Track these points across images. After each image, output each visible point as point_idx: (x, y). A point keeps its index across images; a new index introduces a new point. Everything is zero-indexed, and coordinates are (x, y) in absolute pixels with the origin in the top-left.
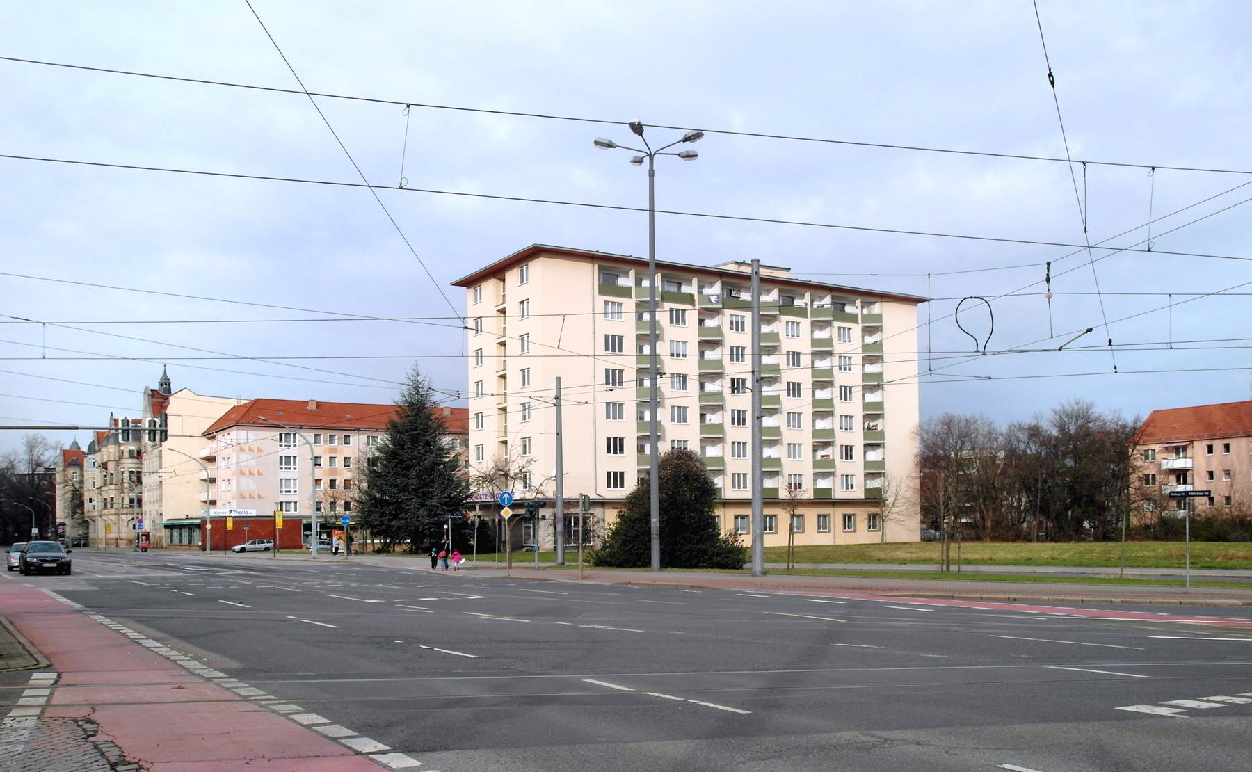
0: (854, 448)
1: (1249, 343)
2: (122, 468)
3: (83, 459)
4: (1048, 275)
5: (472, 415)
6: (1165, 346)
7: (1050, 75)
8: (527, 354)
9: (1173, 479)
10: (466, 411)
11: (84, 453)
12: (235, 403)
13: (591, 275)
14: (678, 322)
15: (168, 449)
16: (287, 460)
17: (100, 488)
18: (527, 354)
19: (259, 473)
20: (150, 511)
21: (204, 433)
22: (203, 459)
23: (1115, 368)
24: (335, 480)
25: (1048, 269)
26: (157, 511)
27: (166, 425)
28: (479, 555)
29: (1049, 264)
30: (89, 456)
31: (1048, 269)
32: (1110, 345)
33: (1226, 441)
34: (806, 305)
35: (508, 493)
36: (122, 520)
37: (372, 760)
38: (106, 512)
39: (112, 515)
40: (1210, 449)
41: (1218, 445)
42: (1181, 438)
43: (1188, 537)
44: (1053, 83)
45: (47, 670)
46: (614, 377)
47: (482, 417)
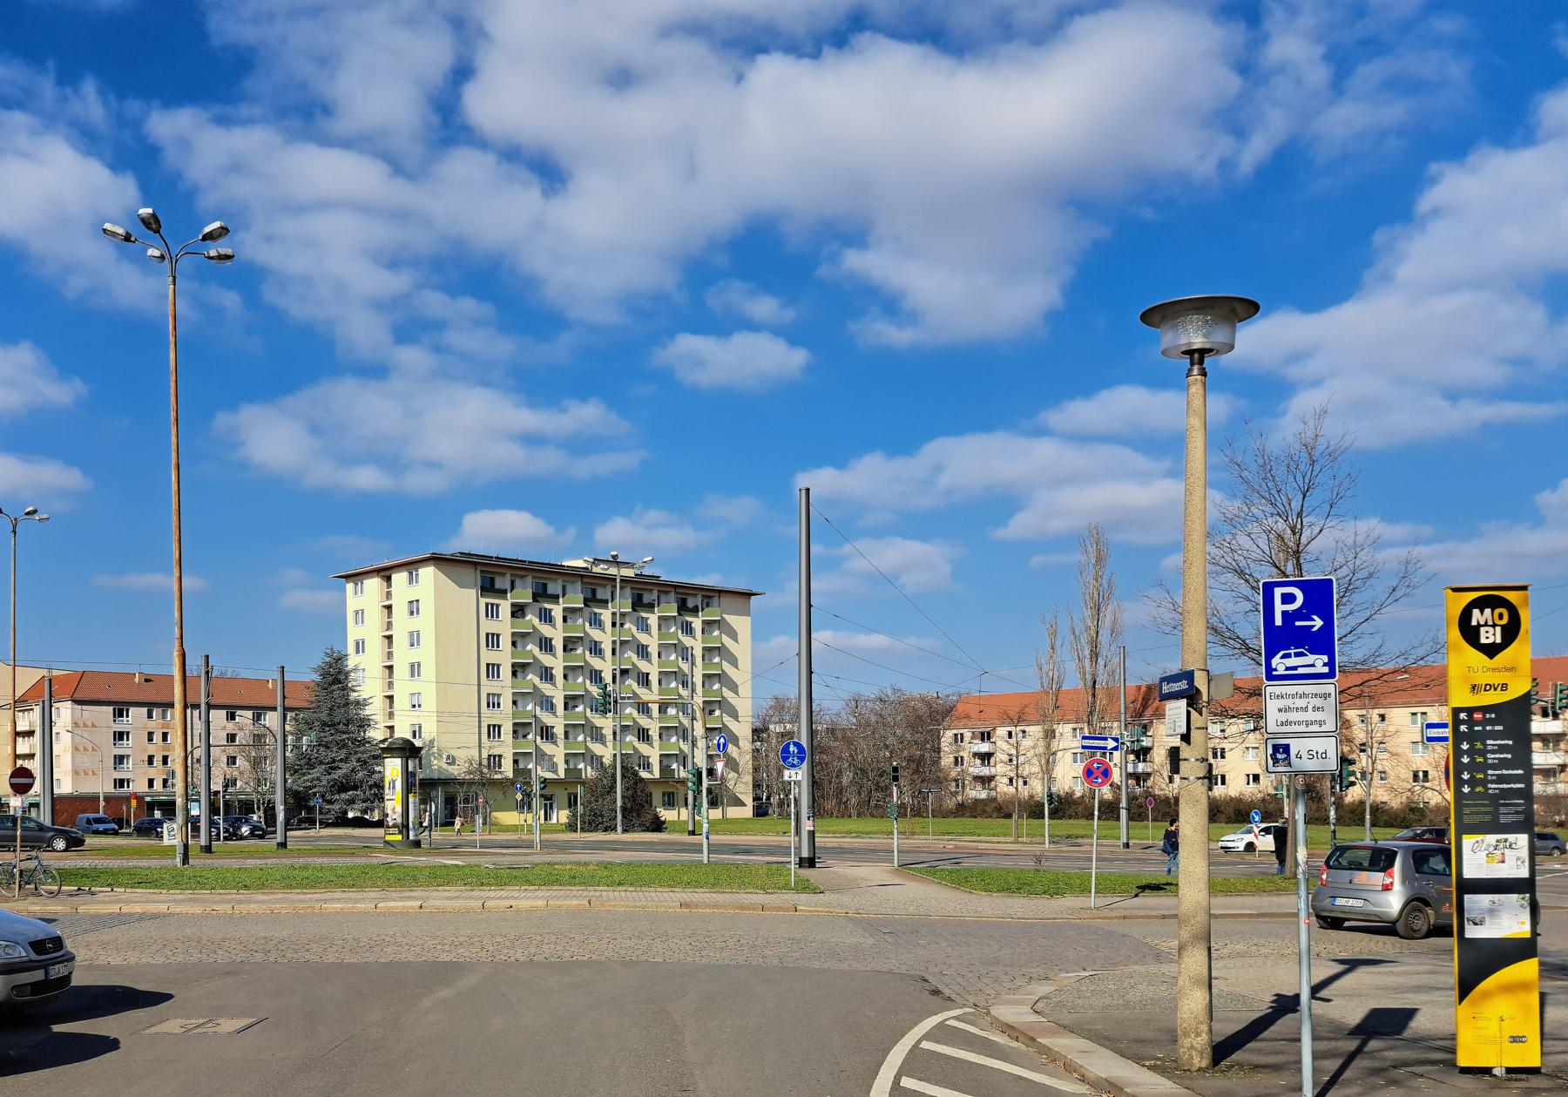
9: (978, 762)
16: (119, 736)
46: (493, 670)
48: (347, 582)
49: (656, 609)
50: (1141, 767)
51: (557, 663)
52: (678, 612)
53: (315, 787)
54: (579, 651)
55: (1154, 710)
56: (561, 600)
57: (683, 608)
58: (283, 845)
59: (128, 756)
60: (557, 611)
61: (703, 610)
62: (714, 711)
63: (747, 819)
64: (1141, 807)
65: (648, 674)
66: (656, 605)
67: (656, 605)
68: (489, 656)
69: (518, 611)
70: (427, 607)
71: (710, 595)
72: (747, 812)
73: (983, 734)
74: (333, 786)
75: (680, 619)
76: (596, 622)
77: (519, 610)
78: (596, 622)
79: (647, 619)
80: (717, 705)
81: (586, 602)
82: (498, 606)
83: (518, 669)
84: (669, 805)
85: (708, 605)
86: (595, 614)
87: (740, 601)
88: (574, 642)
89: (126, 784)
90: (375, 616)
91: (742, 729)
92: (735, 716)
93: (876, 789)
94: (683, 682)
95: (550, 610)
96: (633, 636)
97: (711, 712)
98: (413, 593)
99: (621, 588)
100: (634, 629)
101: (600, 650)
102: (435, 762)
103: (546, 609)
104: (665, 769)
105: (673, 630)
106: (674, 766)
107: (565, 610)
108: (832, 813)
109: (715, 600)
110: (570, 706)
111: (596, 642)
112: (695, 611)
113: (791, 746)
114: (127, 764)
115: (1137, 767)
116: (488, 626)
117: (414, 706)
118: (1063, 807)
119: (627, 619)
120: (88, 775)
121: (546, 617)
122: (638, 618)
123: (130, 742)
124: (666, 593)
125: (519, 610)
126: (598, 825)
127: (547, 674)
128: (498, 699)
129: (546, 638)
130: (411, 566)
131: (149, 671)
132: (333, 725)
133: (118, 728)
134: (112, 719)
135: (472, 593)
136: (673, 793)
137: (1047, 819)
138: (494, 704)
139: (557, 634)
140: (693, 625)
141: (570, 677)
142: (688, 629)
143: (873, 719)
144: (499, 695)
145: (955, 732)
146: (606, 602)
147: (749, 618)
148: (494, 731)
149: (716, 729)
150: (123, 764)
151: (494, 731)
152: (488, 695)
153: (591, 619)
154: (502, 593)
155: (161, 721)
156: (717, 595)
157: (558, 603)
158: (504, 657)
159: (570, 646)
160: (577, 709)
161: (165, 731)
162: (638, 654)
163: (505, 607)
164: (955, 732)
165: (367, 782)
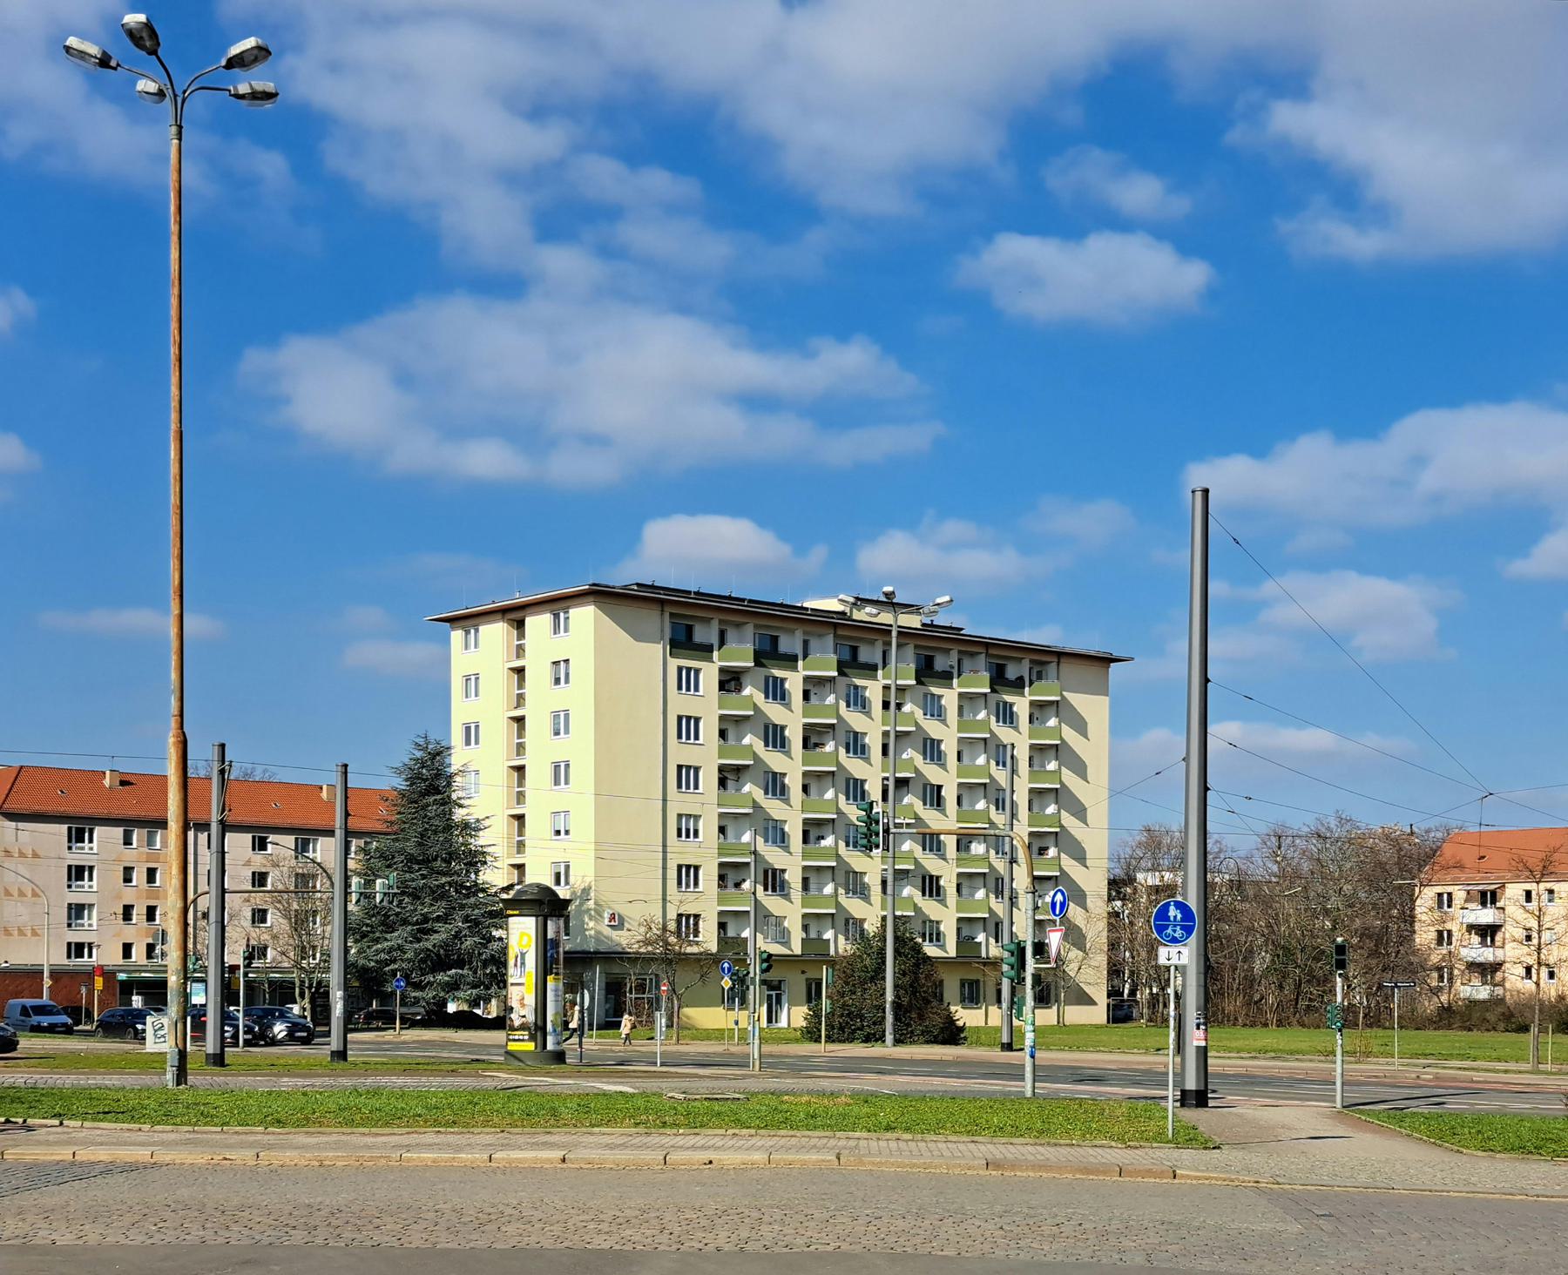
14: (688, 689)
33: (1528, 886)
34: (952, 667)
46: (687, 775)
48: (453, 629)
51: (792, 766)
57: (999, 679)
58: (341, 1055)
59: (91, 906)
60: (794, 681)
61: (1031, 683)
62: (1047, 849)
63: (1097, 1027)
65: (940, 787)
66: (955, 674)
67: (955, 674)
68: (681, 753)
69: (730, 681)
71: (1044, 659)
72: (1098, 1014)
73: (1483, 894)
75: (994, 698)
81: (842, 667)
82: (697, 671)
83: (728, 776)
85: (1040, 677)
86: (856, 687)
87: (1089, 672)
89: (86, 950)
90: (497, 685)
92: (1080, 857)
97: (1042, 851)
98: (560, 647)
99: (899, 646)
100: (919, 713)
106: (981, 938)
108: (1236, 1019)
111: (856, 734)
112: (1018, 685)
113: (1172, 908)
114: (89, 918)
116: (682, 704)
117: (558, 833)
121: (776, 691)
122: (925, 695)
123: (94, 883)
124: (972, 655)
126: (854, 1031)
129: (775, 726)
130: (557, 604)
131: (129, 767)
133: (76, 859)
134: (66, 844)
135: (655, 651)
136: (977, 981)
138: (688, 831)
139: (793, 721)
140: (1015, 709)
141: (813, 789)
143: (1306, 866)
144: (697, 818)
145: (1439, 889)
146: (874, 668)
152: (680, 816)
153: (848, 696)
155: (146, 850)
158: (707, 754)
159: (814, 740)
162: (924, 754)
163: (709, 674)
164: (1439, 889)
165: (480, 954)
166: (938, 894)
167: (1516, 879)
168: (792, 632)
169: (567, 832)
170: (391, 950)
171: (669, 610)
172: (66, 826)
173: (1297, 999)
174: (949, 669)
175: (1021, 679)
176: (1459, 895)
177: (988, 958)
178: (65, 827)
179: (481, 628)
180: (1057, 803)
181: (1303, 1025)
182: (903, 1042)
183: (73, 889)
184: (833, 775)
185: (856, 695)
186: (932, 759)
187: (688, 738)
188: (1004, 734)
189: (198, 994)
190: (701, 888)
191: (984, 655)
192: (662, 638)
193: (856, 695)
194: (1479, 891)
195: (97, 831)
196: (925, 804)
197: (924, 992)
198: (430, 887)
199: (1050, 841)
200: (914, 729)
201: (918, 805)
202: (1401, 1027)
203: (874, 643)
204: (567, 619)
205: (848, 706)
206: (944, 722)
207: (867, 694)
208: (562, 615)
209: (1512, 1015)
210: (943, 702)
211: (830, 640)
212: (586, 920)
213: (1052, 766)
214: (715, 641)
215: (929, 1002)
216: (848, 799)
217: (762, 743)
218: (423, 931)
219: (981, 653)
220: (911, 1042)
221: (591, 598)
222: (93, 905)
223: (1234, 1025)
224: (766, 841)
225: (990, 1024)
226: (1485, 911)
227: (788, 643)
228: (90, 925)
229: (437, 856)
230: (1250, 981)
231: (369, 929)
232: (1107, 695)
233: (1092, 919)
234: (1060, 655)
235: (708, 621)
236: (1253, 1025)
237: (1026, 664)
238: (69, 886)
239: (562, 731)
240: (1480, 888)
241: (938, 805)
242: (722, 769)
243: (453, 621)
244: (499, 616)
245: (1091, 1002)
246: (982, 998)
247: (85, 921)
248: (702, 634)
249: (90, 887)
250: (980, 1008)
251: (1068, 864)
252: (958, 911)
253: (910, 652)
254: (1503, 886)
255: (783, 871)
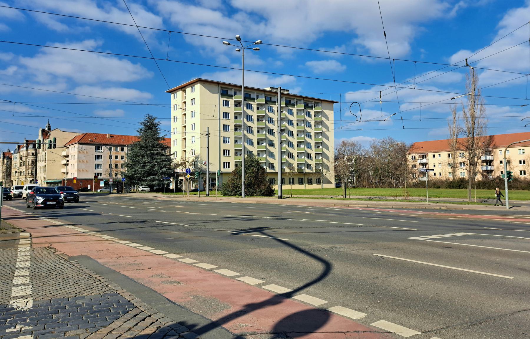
0: (230, 164)
1: (526, 264)
2: (29, 159)
3: (11, 156)
4: (381, 95)
5: (172, 141)
6: (419, 120)
7: (385, 33)
8: (194, 118)
9: (421, 166)
10: (170, 139)
11: (12, 154)
12: (78, 134)
13: (218, 90)
15: (51, 152)
16: (98, 157)
17: (19, 168)
18: (194, 118)
19: (87, 162)
20: (40, 176)
21: (64, 146)
22: (63, 156)
23: (404, 127)
24: (117, 165)
25: (381, 93)
26: (43, 176)
27: (56, 142)
28: (166, 193)
29: (381, 92)
30: (15, 155)
31: (381, 93)
32: (402, 119)
34: (295, 103)
35: (189, 169)
36: (28, 180)
37: (163, 256)
38: (20, 177)
39: (24, 178)
40: (434, 156)
41: (437, 154)
42: (424, 152)
43: (427, 182)
44: (385, 35)
45: (23, 232)
46: (226, 127)
47: (176, 141)
48: (172, 94)
49: (296, 106)
50: (489, 168)
51: (254, 125)
52: (304, 107)
53: (136, 174)
54: (264, 121)
55: (493, 145)
56: (256, 100)
57: (307, 106)
58: (208, 195)
59: (101, 164)
60: (254, 105)
61: (315, 107)
62: (319, 146)
63: (333, 188)
64: (498, 183)
65: (292, 132)
66: (296, 105)
67: (296, 105)
68: (224, 122)
69: (237, 104)
70: (197, 101)
71: (318, 102)
72: (333, 186)
73: (423, 156)
74: (144, 173)
75: (305, 110)
76: (271, 110)
77: (239, 104)
78: (271, 110)
79: (292, 110)
80: (320, 144)
81: (266, 102)
82: (228, 102)
83: (237, 127)
84: (301, 183)
85: (317, 106)
86: (271, 107)
87: (329, 105)
88: (262, 118)
89: (100, 175)
91: (331, 154)
92: (327, 148)
93: (383, 177)
94: (307, 135)
95: (251, 105)
96: (286, 116)
97: (318, 147)
98: (192, 96)
99: (281, 97)
100: (287, 114)
101: (273, 121)
102: (200, 165)
103: (249, 104)
104: (300, 169)
105: (303, 114)
106: (303, 168)
107: (258, 104)
108: (365, 186)
109: (320, 104)
110: (260, 143)
111: (271, 118)
112: (311, 108)
114: (101, 167)
115: (488, 168)
116: (224, 109)
117: (192, 142)
118: (461, 184)
119: (284, 109)
120: (84, 171)
121: (250, 107)
122: (288, 109)
123: (102, 159)
124: (300, 100)
125: (239, 104)
126: (236, 192)
127: (250, 130)
128: (228, 139)
129: (249, 116)
130: (192, 84)
131: (113, 133)
132: (147, 147)
133: (97, 154)
134: (95, 150)
135: (216, 96)
136: (303, 178)
137: (506, 189)
138: (226, 141)
139: (254, 114)
140: (311, 113)
141: (299, 156)
142: (309, 115)
143: (381, 149)
144: (229, 138)
145: (412, 155)
146: (275, 102)
147: (332, 112)
148: (226, 152)
149: (320, 153)
150: (99, 167)
151: (226, 152)
152: (224, 137)
153: (269, 109)
154: (231, 96)
155: (115, 151)
156: (320, 102)
157: (255, 102)
158: (231, 122)
159: (260, 119)
160: (263, 145)
161: (117, 155)
162: (288, 124)
163: (232, 102)
164: (412, 155)
165: (160, 172)
166: (292, 157)
167: (431, 152)
168: (254, 93)
169: (194, 142)
170: (135, 171)
171: (220, 86)
172: (95, 146)
173: (380, 181)
174: (294, 103)
175: (312, 106)
176: (417, 157)
177: (305, 172)
178: (95, 146)
179: (177, 93)
180: (321, 136)
181: (382, 188)
182: (252, 195)
183: (97, 160)
184: (265, 128)
185: (271, 109)
186: (290, 125)
187: (226, 118)
188: (308, 119)
189: (102, 184)
190: (230, 155)
191: (303, 100)
192: (219, 93)
193: (271, 109)
194: (422, 155)
195: (103, 147)
196: (289, 135)
197: (260, 179)
198: (147, 154)
199: (320, 144)
200: (285, 117)
201: (287, 136)
202: (429, 188)
203: (275, 97)
204: (194, 88)
205: (269, 111)
206: (293, 116)
207: (274, 108)
208: (193, 87)
209: (435, 184)
210: (293, 111)
211: (264, 95)
212: (199, 163)
213: (320, 127)
214: (233, 94)
215: (262, 182)
216: (307, 158)
217: (288, 146)
218: (144, 166)
219: (302, 100)
220: (255, 195)
221: (199, 82)
222: (102, 164)
223: (365, 188)
224: (248, 144)
225: (306, 188)
226: (424, 160)
227: (253, 96)
228: (101, 169)
229: (149, 146)
230: (369, 178)
231: (130, 165)
232: (333, 111)
233: (331, 164)
234: (322, 100)
235: (231, 89)
236: (370, 188)
237: (313, 102)
238: (96, 160)
239: (193, 116)
240: (422, 154)
241: (292, 136)
242: (235, 126)
243: (171, 92)
244: (180, 89)
245: (331, 183)
246: (304, 183)
247: (100, 168)
248: (230, 92)
249: (101, 160)
250: (304, 185)
251: (324, 150)
252: (297, 161)
253: (284, 99)
254: (428, 153)
255: (252, 151)
